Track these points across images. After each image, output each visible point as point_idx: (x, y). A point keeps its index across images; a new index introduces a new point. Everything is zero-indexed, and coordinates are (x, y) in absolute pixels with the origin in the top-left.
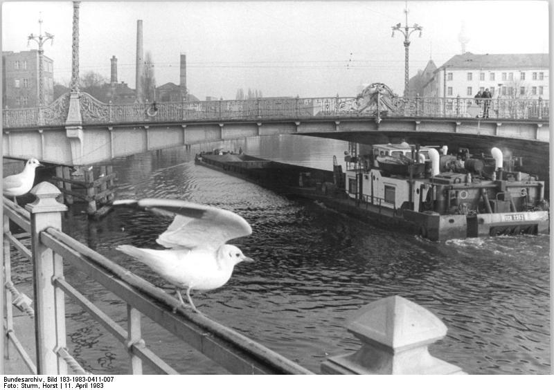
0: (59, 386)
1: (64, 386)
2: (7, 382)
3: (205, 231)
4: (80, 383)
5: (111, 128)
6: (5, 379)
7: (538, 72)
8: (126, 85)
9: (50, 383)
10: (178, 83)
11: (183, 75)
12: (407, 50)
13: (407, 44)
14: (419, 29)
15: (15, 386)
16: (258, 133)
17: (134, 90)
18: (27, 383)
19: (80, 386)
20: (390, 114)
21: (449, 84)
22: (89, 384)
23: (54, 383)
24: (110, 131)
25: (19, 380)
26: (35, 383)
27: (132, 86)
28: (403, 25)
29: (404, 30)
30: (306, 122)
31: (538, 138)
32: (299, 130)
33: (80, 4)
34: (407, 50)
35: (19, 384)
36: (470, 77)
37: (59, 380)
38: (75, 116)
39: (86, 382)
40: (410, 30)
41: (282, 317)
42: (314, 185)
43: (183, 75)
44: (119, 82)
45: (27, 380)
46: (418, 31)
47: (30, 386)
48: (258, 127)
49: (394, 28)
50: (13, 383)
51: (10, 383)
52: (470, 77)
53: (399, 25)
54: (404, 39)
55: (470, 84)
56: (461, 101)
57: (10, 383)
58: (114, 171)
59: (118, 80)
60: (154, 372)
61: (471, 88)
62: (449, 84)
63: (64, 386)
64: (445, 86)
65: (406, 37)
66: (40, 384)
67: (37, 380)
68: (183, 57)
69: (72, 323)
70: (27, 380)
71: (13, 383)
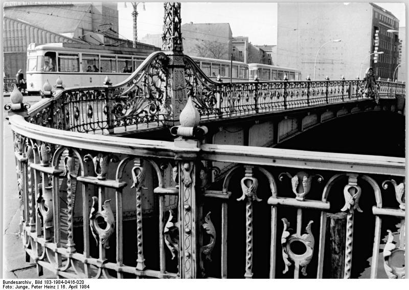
0: (43, 287)
2: (5, 284)
4: (72, 285)
6: (4, 282)
9: (39, 285)
12: (135, 20)
18: (20, 285)
19: (72, 287)
21: (182, 177)
22: (79, 285)
25: (14, 282)
26: (25, 285)
33: (253, 44)
34: (135, 20)
35: (15, 285)
37: (43, 282)
39: (76, 284)
41: (337, 261)
42: (204, 111)
45: (20, 283)
50: (10, 285)
51: (7, 285)
54: (132, 10)
57: (7, 285)
60: (117, 155)
62: (182, 177)
66: (29, 286)
67: (27, 283)
69: (4, 4)
70: (20, 283)
71: (10, 285)
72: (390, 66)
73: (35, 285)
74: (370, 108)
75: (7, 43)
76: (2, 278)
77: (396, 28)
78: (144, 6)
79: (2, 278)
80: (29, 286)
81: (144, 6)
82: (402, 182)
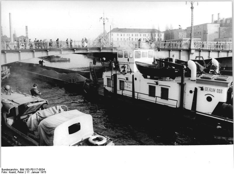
0: (24, 172)
1: (26, 172)
3: (185, 92)
5: (5, 52)
6: (2, 169)
7: (145, 34)
8: (6, 36)
9: (22, 171)
10: (25, 36)
11: (27, 33)
12: (104, 26)
13: (104, 24)
14: (108, 19)
15: (6, 172)
16: (61, 53)
17: (9, 38)
18: (11, 171)
20: (104, 46)
23: (23, 171)
24: (19, 52)
26: (14, 171)
27: (9, 36)
28: (103, 18)
29: (103, 19)
30: (77, 49)
31: (22, 59)
32: (76, 52)
34: (104, 26)
35: (8, 171)
36: (118, 35)
37: (25, 170)
38: (34, 47)
40: (105, 19)
43: (27, 33)
44: (4, 35)
46: (107, 20)
47: (13, 172)
48: (19, 52)
49: (100, 19)
50: (6, 171)
51: (4, 171)
52: (118, 35)
53: (102, 18)
54: (191, 6)
55: (118, 37)
56: (76, 42)
57: (4, 171)
58: (8, 68)
59: (3, 34)
61: (118, 38)
63: (26, 172)
64: (111, 37)
65: (104, 22)
66: (17, 171)
67: (16, 170)
68: (26, 27)
71: (6, 171)
72: (194, 74)
73: (20, 171)
74: (114, 67)
75: (5, 69)
76: (1, 167)
77: (128, 55)
78: (198, 3)
79: (1, 167)
80: (17, 171)
81: (198, 3)
82: (111, 71)
